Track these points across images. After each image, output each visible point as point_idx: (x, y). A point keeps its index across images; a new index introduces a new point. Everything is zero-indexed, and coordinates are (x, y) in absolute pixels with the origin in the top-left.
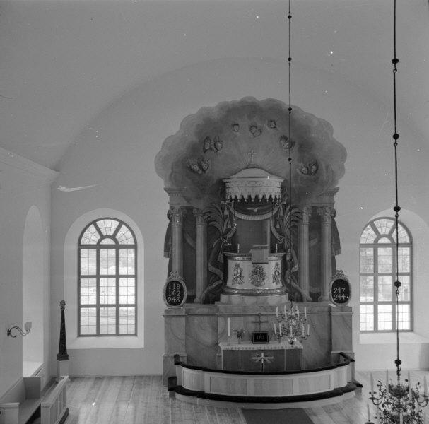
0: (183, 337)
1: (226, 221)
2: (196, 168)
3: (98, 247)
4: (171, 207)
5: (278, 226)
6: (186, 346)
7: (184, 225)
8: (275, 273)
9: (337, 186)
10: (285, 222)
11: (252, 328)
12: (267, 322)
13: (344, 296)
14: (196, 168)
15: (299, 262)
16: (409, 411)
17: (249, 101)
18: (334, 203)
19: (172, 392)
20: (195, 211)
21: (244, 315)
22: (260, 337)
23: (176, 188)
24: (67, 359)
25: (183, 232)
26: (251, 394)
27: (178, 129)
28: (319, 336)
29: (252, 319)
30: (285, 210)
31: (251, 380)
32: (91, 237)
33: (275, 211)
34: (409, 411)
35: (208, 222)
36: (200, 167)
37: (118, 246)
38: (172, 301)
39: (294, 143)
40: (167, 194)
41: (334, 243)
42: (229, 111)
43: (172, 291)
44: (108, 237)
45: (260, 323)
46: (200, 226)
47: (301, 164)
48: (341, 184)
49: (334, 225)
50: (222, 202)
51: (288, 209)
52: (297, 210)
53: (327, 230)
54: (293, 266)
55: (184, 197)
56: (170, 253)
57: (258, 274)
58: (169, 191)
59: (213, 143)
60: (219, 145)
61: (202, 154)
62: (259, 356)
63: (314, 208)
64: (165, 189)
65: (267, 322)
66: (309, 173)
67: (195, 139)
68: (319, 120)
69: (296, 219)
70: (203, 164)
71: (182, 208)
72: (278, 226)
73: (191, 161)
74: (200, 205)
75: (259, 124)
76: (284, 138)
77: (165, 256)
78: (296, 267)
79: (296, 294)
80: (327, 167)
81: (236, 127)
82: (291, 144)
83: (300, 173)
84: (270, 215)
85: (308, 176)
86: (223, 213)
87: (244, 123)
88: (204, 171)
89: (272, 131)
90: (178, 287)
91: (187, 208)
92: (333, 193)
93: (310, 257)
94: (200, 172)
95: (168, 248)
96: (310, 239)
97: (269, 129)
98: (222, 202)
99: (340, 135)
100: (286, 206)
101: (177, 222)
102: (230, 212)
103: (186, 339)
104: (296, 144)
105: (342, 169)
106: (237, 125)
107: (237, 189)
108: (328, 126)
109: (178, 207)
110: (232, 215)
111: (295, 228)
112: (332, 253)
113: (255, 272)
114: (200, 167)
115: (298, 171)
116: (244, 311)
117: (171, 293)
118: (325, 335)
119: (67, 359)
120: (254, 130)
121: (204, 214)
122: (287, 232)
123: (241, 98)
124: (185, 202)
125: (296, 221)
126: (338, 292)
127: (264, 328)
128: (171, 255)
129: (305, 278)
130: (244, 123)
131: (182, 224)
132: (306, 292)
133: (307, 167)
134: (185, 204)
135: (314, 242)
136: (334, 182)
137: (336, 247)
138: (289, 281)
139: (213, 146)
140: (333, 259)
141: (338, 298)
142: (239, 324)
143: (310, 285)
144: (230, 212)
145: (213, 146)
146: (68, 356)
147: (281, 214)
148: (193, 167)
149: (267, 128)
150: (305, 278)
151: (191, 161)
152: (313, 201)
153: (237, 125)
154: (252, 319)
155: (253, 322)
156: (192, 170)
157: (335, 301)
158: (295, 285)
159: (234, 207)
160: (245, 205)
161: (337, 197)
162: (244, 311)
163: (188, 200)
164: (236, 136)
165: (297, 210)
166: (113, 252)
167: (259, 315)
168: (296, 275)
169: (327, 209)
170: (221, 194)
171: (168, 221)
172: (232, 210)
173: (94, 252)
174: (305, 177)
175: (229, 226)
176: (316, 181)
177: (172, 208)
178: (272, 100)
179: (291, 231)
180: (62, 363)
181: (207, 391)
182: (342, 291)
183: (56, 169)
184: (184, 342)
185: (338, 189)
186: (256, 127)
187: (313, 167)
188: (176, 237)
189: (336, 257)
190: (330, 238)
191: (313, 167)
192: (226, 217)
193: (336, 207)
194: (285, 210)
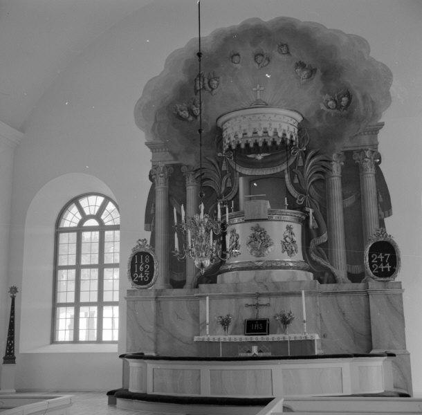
0: (151, 327)
1: (225, 178)
2: (185, 114)
3: (79, 230)
4: (153, 166)
5: (296, 181)
6: (156, 343)
7: (170, 188)
8: (285, 239)
9: (381, 121)
10: (306, 174)
11: (248, 314)
12: (268, 305)
13: (388, 267)
14: (185, 114)
15: (329, 230)
16: (204, 243)
17: (253, 24)
18: (377, 145)
19: (112, 397)
20: (184, 169)
21: (235, 296)
22: (256, 326)
23: (159, 141)
24: (14, 363)
25: (169, 197)
26: (206, 393)
27: (162, 68)
28: (352, 328)
29: (248, 301)
30: (304, 159)
31: (206, 369)
32: (72, 218)
33: (292, 161)
34: (204, 243)
35: (201, 179)
36: (191, 112)
37: (102, 228)
38: (139, 279)
39: (315, 70)
40: (149, 150)
41: (381, 200)
42: (226, 40)
43: (139, 264)
44: (91, 217)
45: (257, 306)
46: (191, 187)
47: (327, 97)
48: (386, 117)
49: (379, 176)
50: (219, 154)
51: (309, 157)
52: (320, 157)
53: (370, 182)
54: (319, 234)
55: (170, 152)
56: (152, 224)
57: (260, 240)
58: (151, 146)
59: (206, 81)
60: (215, 82)
61: (194, 96)
62: (249, 352)
63: (348, 154)
64: (147, 144)
65: (268, 305)
66: (338, 106)
67: (182, 77)
68: (348, 36)
69: (322, 169)
70: (195, 109)
71: (167, 167)
72: (296, 181)
73: (179, 106)
74: (191, 161)
75: (266, 51)
76: (301, 65)
77: (146, 229)
78: (325, 236)
79: (327, 274)
80: (364, 97)
81: (236, 58)
82: (312, 72)
83: (325, 109)
84: (284, 167)
85: (336, 111)
86: (220, 169)
87: (247, 51)
88: (195, 117)
89: (284, 58)
90: (147, 260)
91: (173, 165)
92: (375, 131)
93: (346, 223)
94: (191, 118)
95: (150, 218)
96: (344, 197)
97: (281, 57)
98: (219, 154)
99: (378, 53)
100: (306, 153)
101: (161, 181)
102: (229, 166)
103: (157, 334)
104: (319, 70)
105: (387, 97)
106: (238, 55)
107: (236, 129)
108: (362, 41)
109: (162, 165)
110: (232, 171)
111: (322, 179)
112: (379, 215)
113: (254, 237)
114: (191, 112)
115: (323, 107)
116: (236, 290)
117: (138, 267)
118: (362, 328)
119: (14, 363)
120: (260, 58)
121: (196, 170)
122: (308, 186)
123: (242, 21)
124: (172, 158)
125: (323, 173)
126: (379, 259)
127: (263, 314)
128: (154, 226)
129: (340, 251)
130: (247, 51)
131: (167, 187)
132: (341, 272)
133: (336, 102)
134: (171, 160)
135: (350, 201)
136: (376, 115)
137: (385, 205)
138: (314, 257)
139: (207, 85)
140: (382, 224)
141: (380, 269)
142: (228, 308)
143: (347, 263)
144: (229, 166)
145: (207, 85)
146: (15, 358)
147: (300, 163)
148: (181, 113)
149: (276, 54)
150: (340, 251)
151: (179, 106)
152: (347, 144)
153: (238, 55)
154: (248, 301)
155: (247, 305)
156: (180, 117)
157: (374, 274)
158: (323, 263)
159: (235, 160)
160: (243, 153)
161: (382, 137)
162: (236, 290)
163: (175, 156)
164: (236, 69)
165: (320, 157)
166: (96, 234)
167: (259, 295)
168: (326, 248)
169: (368, 154)
170: (217, 144)
171: (150, 183)
172: (233, 164)
173: (73, 236)
174: (333, 112)
175: (229, 185)
176: (349, 117)
177: (155, 167)
178: (283, 19)
179: (315, 187)
180: (9, 367)
181: (150, 392)
182: (384, 259)
183: (22, 130)
184: (152, 336)
185: (382, 125)
186: (263, 55)
187: (343, 99)
188: (160, 204)
189: (387, 220)
190: (374, 194)
191: (343, 99)
192: (224, 173)
193: (381, 149)
194: (304, 159)
